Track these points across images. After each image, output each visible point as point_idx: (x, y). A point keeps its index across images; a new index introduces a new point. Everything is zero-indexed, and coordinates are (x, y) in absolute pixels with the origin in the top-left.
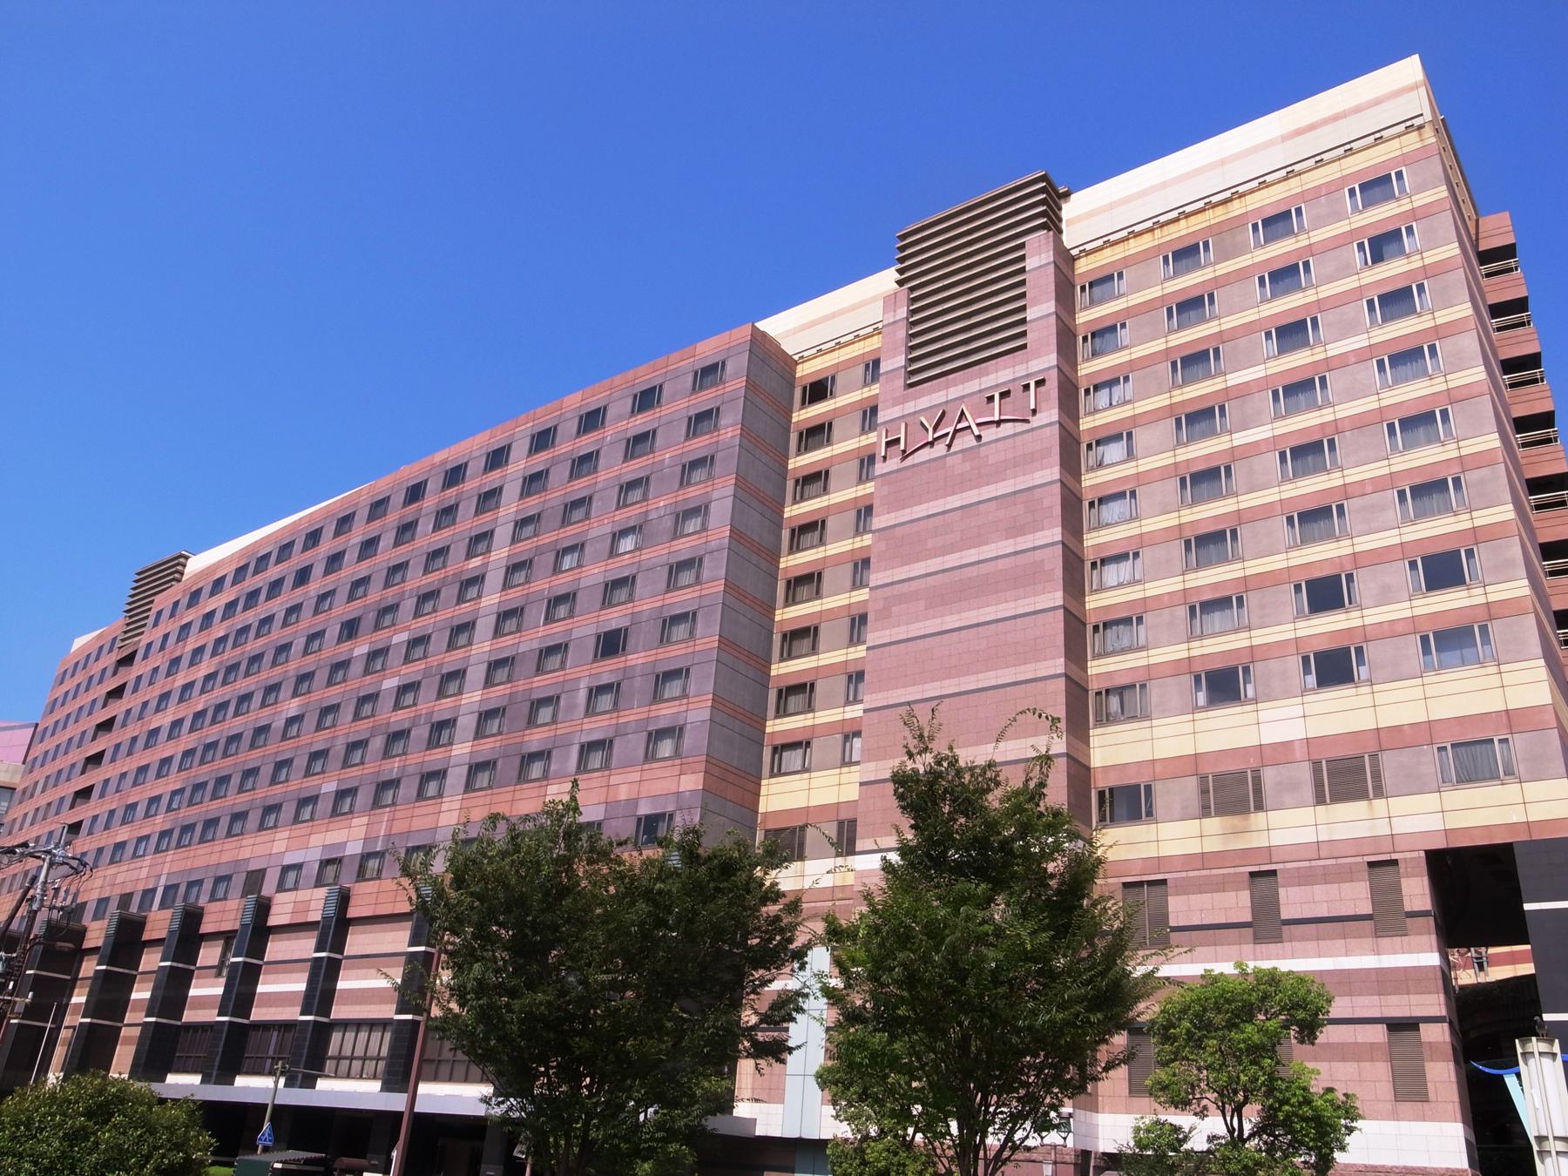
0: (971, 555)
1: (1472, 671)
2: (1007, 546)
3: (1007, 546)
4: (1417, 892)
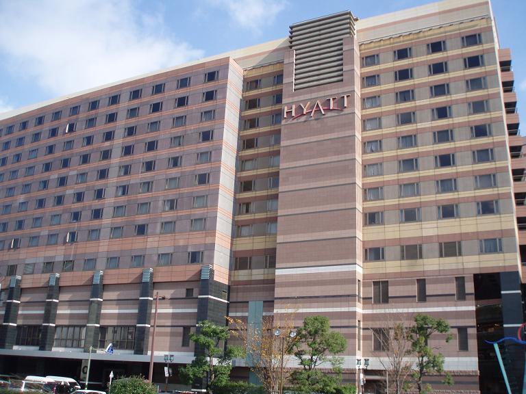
0: (321, 160)
1: (453, 220)
2: (335, 158)
3: (335, 158)
4: (470, 287)
